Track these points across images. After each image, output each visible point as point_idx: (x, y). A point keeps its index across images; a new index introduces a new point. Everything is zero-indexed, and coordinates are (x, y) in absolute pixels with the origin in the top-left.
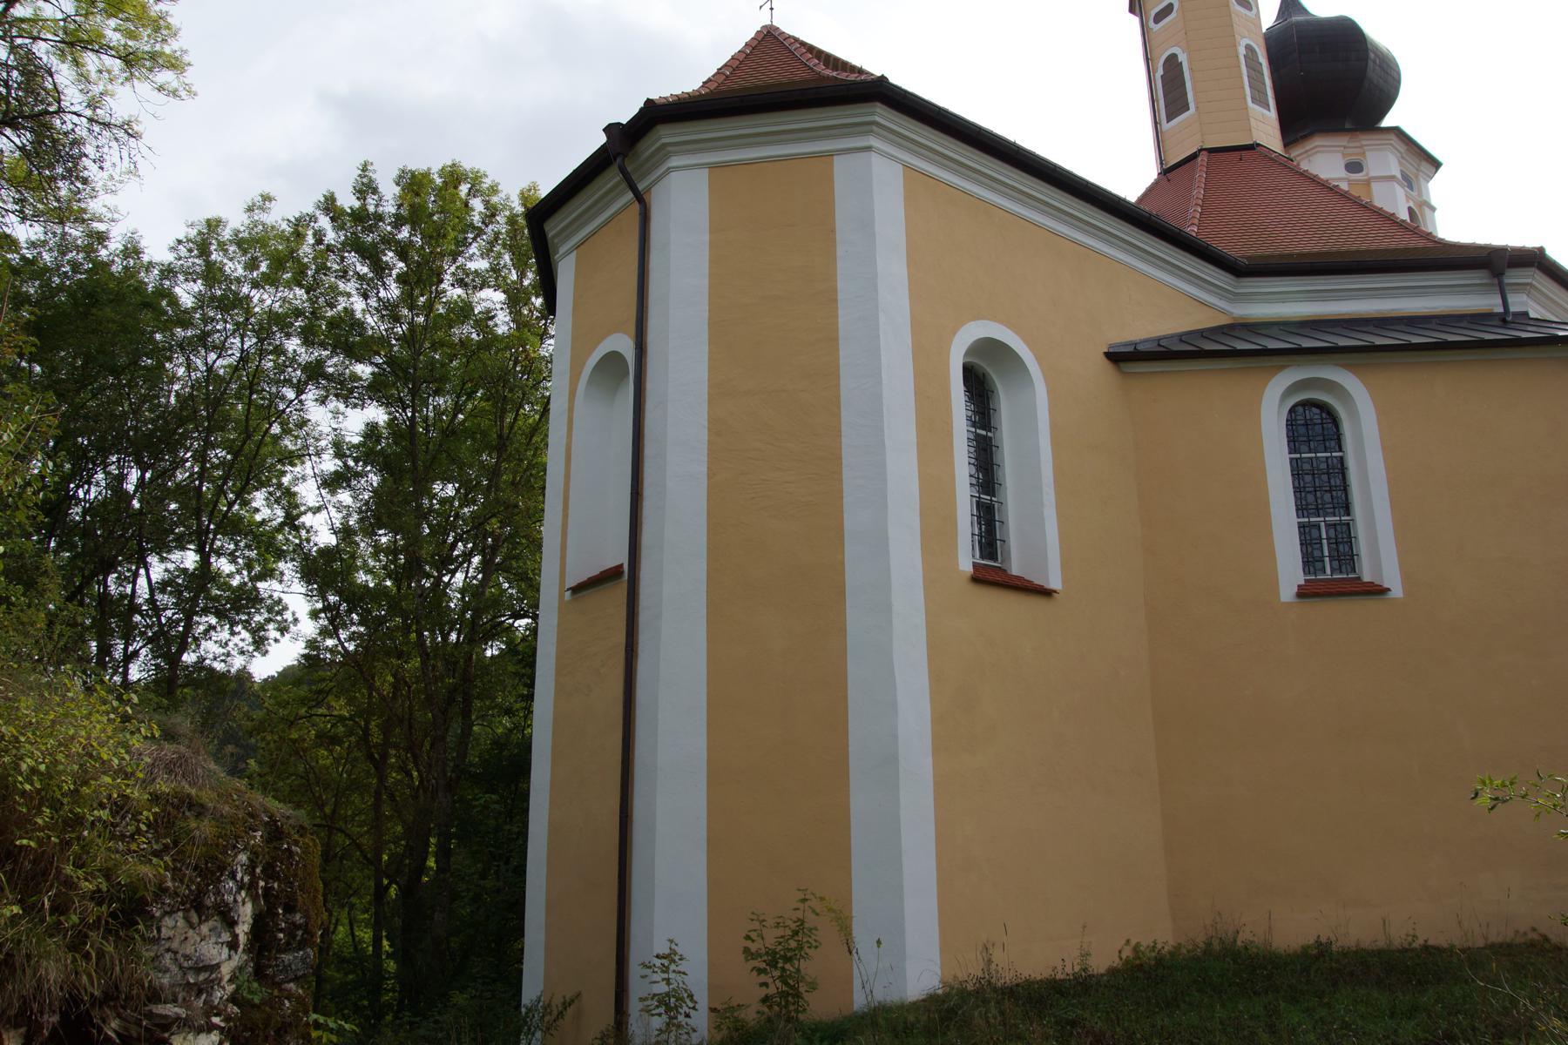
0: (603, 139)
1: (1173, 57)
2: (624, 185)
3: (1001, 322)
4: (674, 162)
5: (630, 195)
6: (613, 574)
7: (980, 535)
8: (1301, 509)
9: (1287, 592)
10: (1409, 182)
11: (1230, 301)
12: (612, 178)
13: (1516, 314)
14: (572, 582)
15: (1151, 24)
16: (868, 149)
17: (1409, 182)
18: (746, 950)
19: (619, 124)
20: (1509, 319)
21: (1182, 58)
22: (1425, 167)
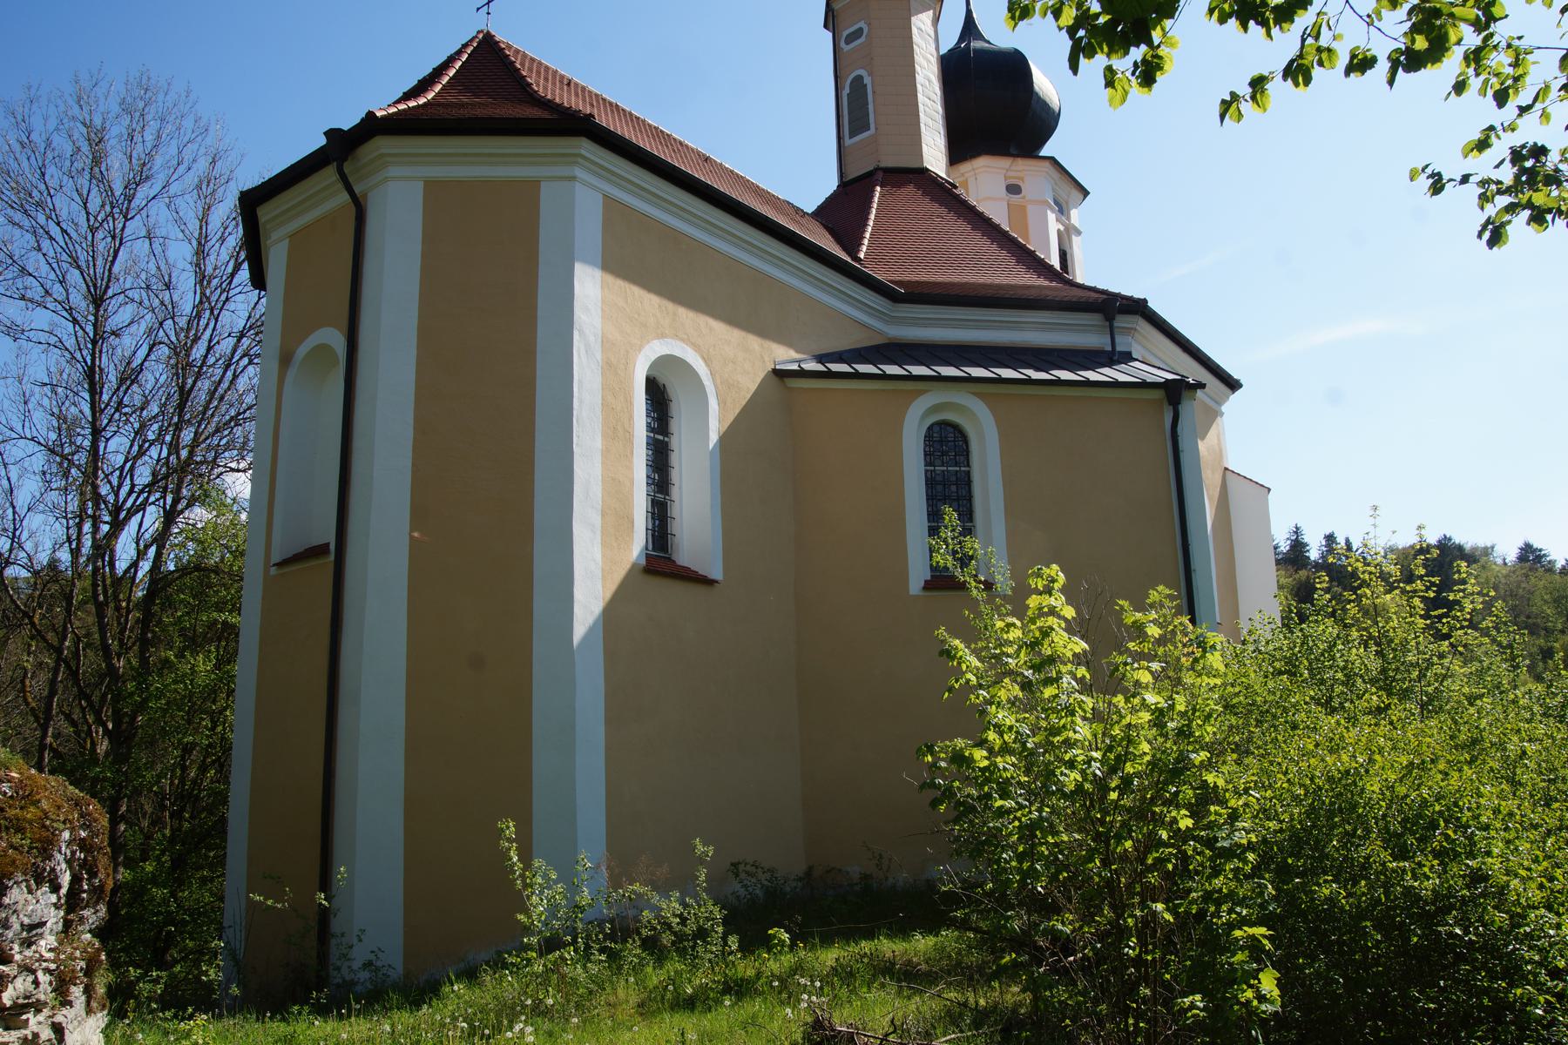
0: (323, 141)
1: (859, 78)
2: (340, 185)
4: (393, 171)
5: (345, 197)
6: (319, 551)
9: (916, 583)
10: (1062, 210)
11: (886, 322)
12: (329, 175)
14: (276, 557)
15: (842, 44)
16: (573, 178)
17: (1062, 210)
18: (1559, 184)
19: (340, 130)
21: (867, 80)
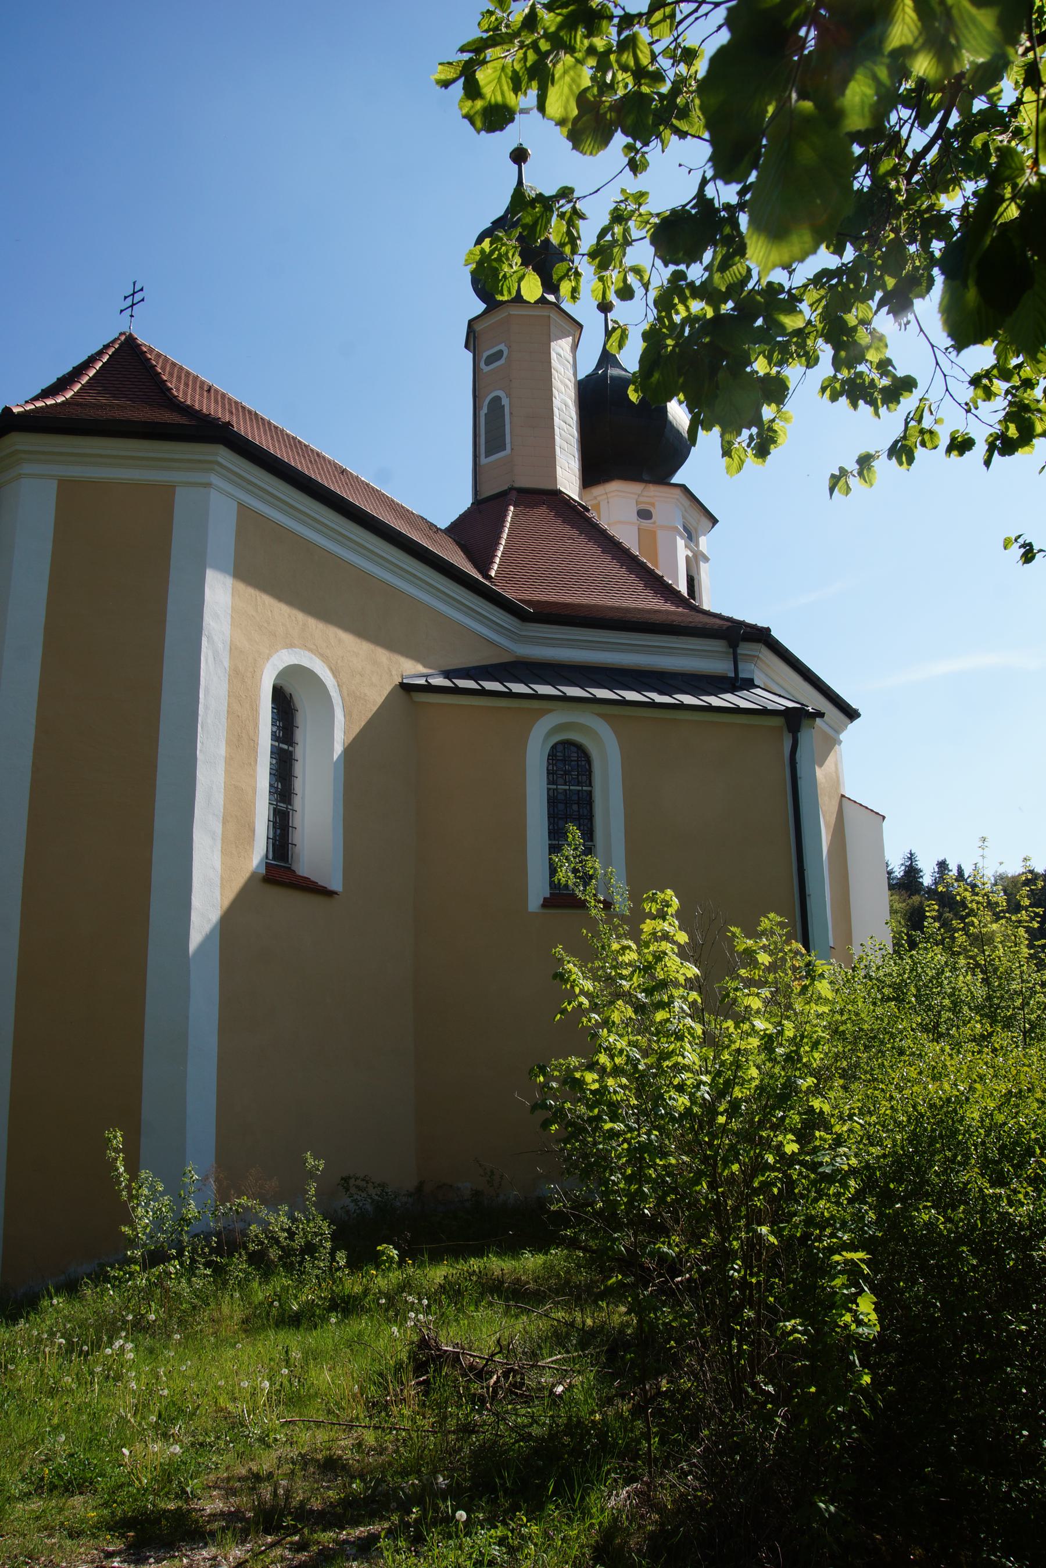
1: (498, 399)
3: (310, 650)
4: (27, 468)
7: (274, 839)
8: (590, 794)
10: (691, 536)
13: (743, 679)
15: (482, 365)
16: (208, 485)
20: (738, 684)
21: (505, 401)
22: (706, 522)
